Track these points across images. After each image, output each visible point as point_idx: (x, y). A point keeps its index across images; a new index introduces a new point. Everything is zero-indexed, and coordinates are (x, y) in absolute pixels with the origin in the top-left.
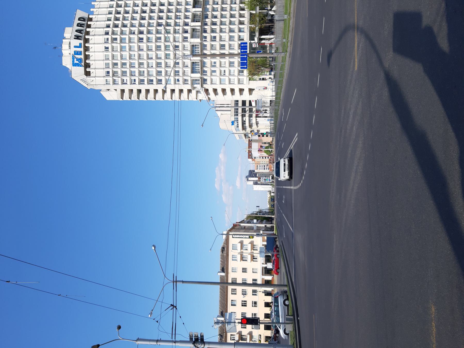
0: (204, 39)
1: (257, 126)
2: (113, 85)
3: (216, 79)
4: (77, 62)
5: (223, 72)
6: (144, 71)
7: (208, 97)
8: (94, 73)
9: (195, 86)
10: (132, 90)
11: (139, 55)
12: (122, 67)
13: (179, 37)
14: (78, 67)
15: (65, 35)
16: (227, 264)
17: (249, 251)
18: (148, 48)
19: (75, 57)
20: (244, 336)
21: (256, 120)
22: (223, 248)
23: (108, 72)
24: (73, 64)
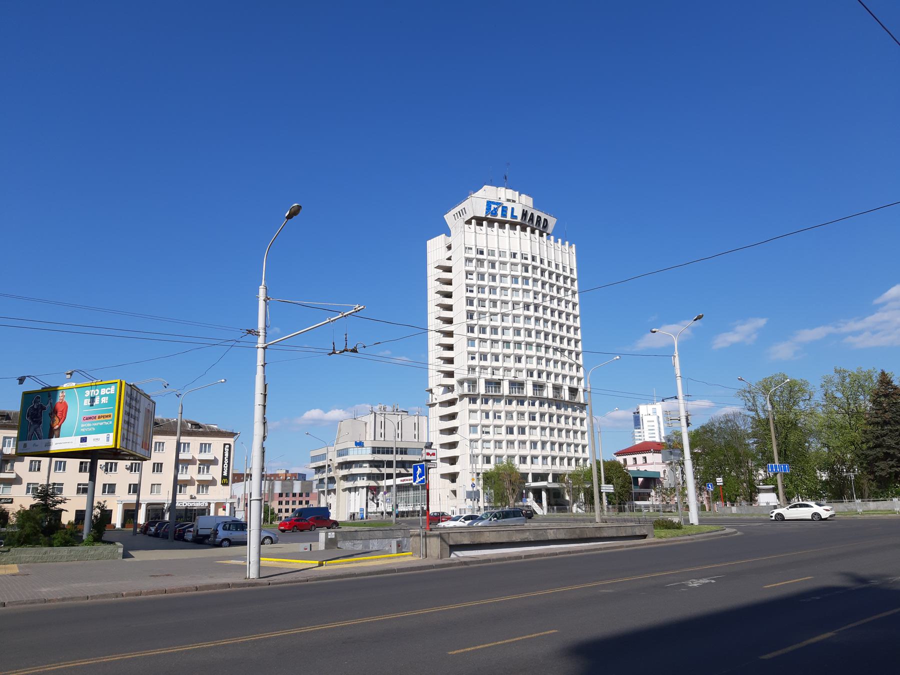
0: (530, 401)
1: (344, 490)
2: (465, 257)
3: (477, 419)
4: (492, 209)
5: (487, 430)
6: (485, 307)
7: (436, 404)
8: (481, 232)
9: (466, 385)
10: (451, 284)
11: (506, 303)
12: (490, 275)
13: (533, 365)
14: (485, 209)
15: (523, 196)
16: (6, 427)
17: (197, 477)
18: (516, 317)
19: (499, 207)
20: (12, 466)
21: (363, 487)
22: (197, 425)
23: (482, 253)
24: (490, 202)
